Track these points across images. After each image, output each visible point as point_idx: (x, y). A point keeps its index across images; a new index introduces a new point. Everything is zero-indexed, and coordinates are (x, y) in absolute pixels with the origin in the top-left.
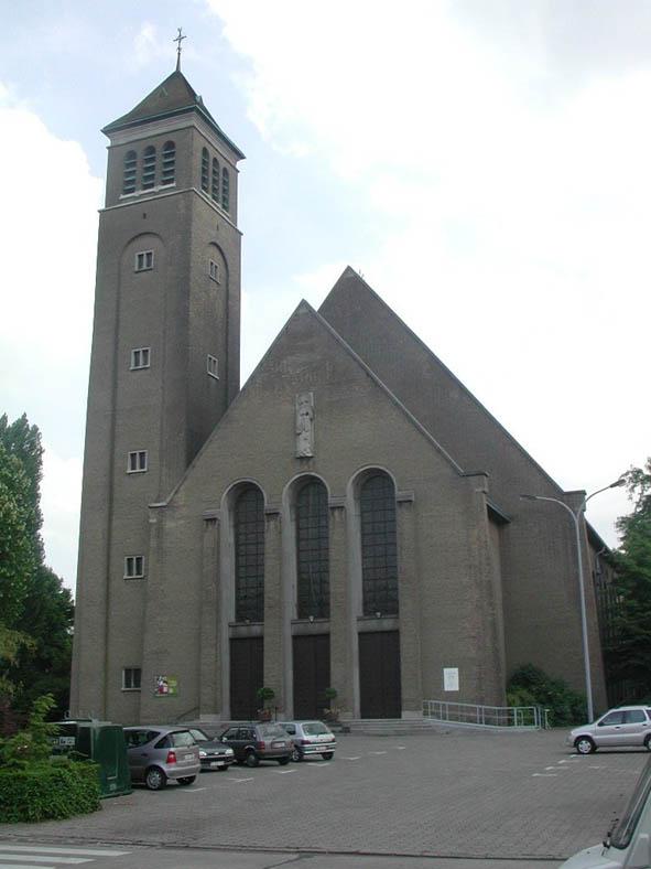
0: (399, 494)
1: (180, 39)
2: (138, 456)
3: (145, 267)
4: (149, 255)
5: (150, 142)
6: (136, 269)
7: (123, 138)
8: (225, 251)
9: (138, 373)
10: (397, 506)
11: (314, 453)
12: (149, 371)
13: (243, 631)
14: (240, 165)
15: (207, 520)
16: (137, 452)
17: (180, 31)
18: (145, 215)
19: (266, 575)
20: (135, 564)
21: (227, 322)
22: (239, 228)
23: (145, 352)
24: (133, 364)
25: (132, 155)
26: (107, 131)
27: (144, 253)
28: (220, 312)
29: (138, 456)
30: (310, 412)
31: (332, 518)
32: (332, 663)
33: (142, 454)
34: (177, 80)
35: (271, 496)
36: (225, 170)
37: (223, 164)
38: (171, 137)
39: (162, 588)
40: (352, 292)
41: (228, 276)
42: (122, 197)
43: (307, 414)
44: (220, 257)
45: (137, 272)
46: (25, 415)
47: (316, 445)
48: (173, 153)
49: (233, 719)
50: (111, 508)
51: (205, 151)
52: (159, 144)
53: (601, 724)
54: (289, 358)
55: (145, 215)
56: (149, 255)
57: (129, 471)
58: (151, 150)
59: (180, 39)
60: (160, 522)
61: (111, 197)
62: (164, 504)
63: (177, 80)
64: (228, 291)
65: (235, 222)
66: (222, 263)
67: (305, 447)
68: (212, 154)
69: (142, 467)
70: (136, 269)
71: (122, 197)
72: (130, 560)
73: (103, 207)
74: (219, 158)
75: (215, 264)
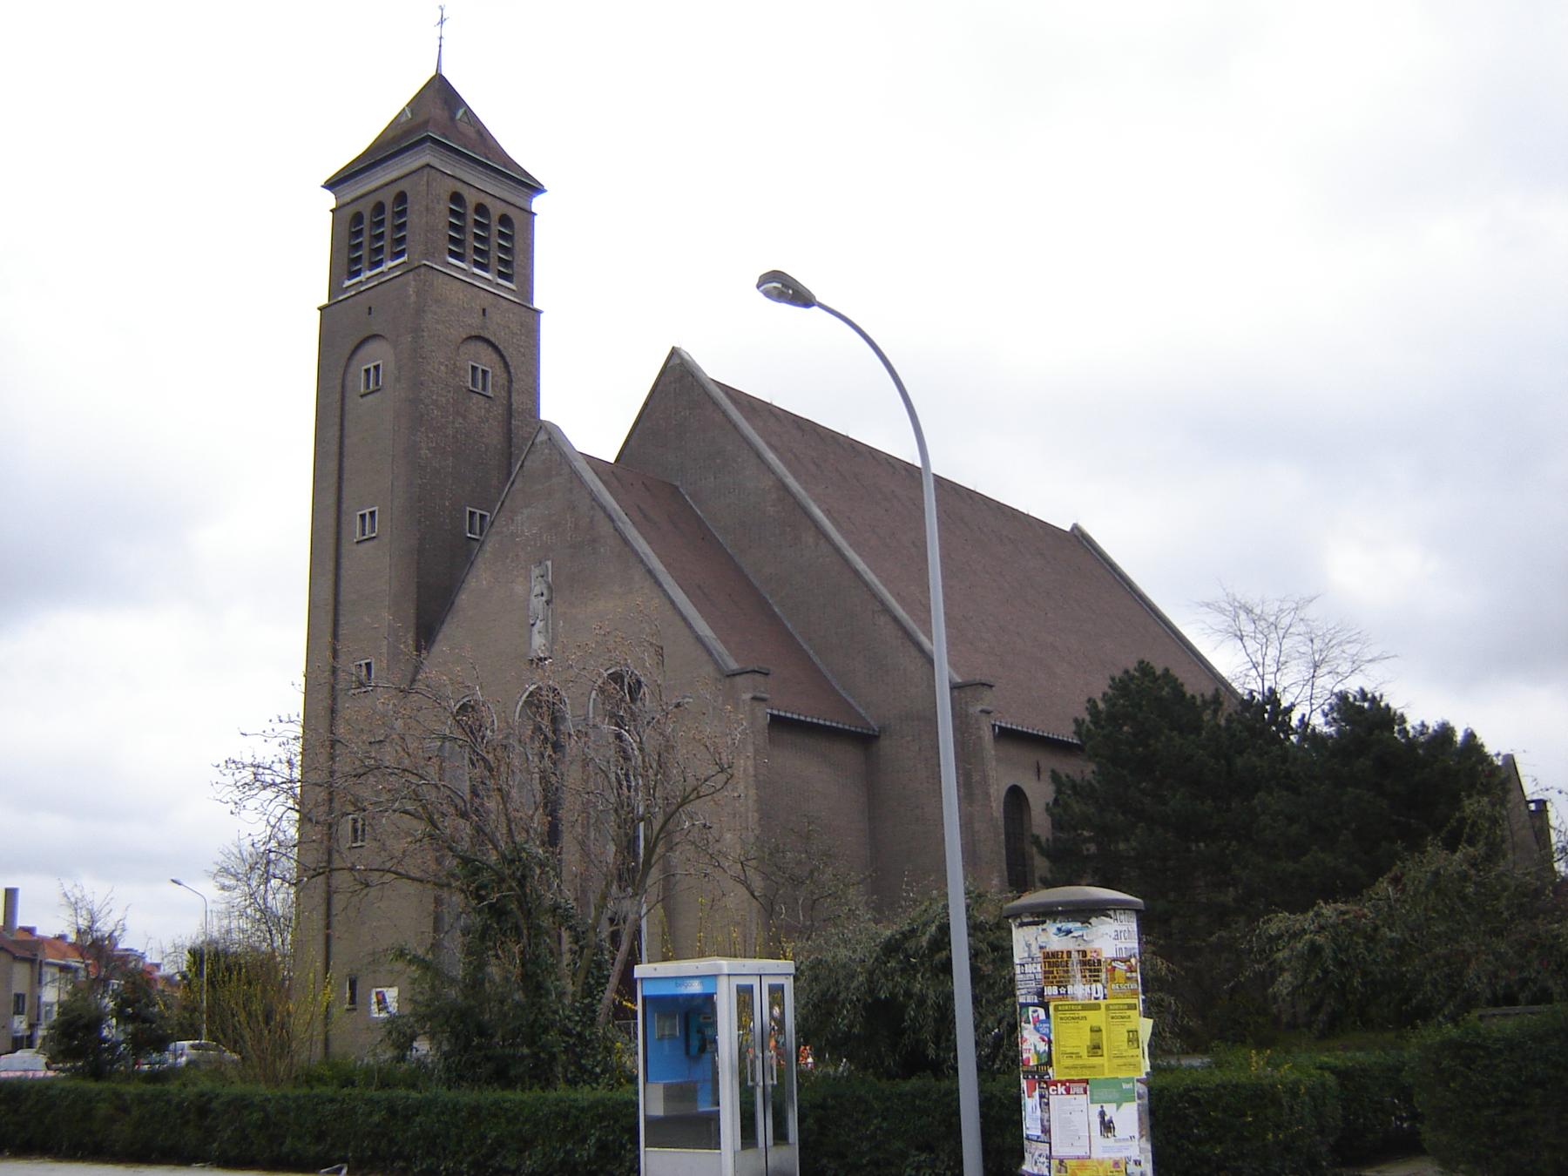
2: (368, 516)
4: (377, 368)
5: (379, 197)
6: (362, 390)
9: (367, 544)
14: (538, 203)
22: (537, 305)
23: (372, 514)
25: (358, 218)
27: (363, 662)
28: (494, 439)
29: (368, 516)
30: (545, 592)
34: (439, 93)
36: (505, 220)
37: (496, 209)
38: (403, 186)
41: (510, 381)
42: (348, 283)
43: (542, 595)
44: (495, 356)
45: (362, 396)
46: (323, 186)
51: (456, 198)
52: (388, 197)
58: (379, 208)
63: (439, 93)
64: (510, 405)
66: (499, 367)
68: (472, 198)
70: (362, 390)
71: (348, 283)
73: (334, 206)
74: (487, 201)
75: (480, 367)
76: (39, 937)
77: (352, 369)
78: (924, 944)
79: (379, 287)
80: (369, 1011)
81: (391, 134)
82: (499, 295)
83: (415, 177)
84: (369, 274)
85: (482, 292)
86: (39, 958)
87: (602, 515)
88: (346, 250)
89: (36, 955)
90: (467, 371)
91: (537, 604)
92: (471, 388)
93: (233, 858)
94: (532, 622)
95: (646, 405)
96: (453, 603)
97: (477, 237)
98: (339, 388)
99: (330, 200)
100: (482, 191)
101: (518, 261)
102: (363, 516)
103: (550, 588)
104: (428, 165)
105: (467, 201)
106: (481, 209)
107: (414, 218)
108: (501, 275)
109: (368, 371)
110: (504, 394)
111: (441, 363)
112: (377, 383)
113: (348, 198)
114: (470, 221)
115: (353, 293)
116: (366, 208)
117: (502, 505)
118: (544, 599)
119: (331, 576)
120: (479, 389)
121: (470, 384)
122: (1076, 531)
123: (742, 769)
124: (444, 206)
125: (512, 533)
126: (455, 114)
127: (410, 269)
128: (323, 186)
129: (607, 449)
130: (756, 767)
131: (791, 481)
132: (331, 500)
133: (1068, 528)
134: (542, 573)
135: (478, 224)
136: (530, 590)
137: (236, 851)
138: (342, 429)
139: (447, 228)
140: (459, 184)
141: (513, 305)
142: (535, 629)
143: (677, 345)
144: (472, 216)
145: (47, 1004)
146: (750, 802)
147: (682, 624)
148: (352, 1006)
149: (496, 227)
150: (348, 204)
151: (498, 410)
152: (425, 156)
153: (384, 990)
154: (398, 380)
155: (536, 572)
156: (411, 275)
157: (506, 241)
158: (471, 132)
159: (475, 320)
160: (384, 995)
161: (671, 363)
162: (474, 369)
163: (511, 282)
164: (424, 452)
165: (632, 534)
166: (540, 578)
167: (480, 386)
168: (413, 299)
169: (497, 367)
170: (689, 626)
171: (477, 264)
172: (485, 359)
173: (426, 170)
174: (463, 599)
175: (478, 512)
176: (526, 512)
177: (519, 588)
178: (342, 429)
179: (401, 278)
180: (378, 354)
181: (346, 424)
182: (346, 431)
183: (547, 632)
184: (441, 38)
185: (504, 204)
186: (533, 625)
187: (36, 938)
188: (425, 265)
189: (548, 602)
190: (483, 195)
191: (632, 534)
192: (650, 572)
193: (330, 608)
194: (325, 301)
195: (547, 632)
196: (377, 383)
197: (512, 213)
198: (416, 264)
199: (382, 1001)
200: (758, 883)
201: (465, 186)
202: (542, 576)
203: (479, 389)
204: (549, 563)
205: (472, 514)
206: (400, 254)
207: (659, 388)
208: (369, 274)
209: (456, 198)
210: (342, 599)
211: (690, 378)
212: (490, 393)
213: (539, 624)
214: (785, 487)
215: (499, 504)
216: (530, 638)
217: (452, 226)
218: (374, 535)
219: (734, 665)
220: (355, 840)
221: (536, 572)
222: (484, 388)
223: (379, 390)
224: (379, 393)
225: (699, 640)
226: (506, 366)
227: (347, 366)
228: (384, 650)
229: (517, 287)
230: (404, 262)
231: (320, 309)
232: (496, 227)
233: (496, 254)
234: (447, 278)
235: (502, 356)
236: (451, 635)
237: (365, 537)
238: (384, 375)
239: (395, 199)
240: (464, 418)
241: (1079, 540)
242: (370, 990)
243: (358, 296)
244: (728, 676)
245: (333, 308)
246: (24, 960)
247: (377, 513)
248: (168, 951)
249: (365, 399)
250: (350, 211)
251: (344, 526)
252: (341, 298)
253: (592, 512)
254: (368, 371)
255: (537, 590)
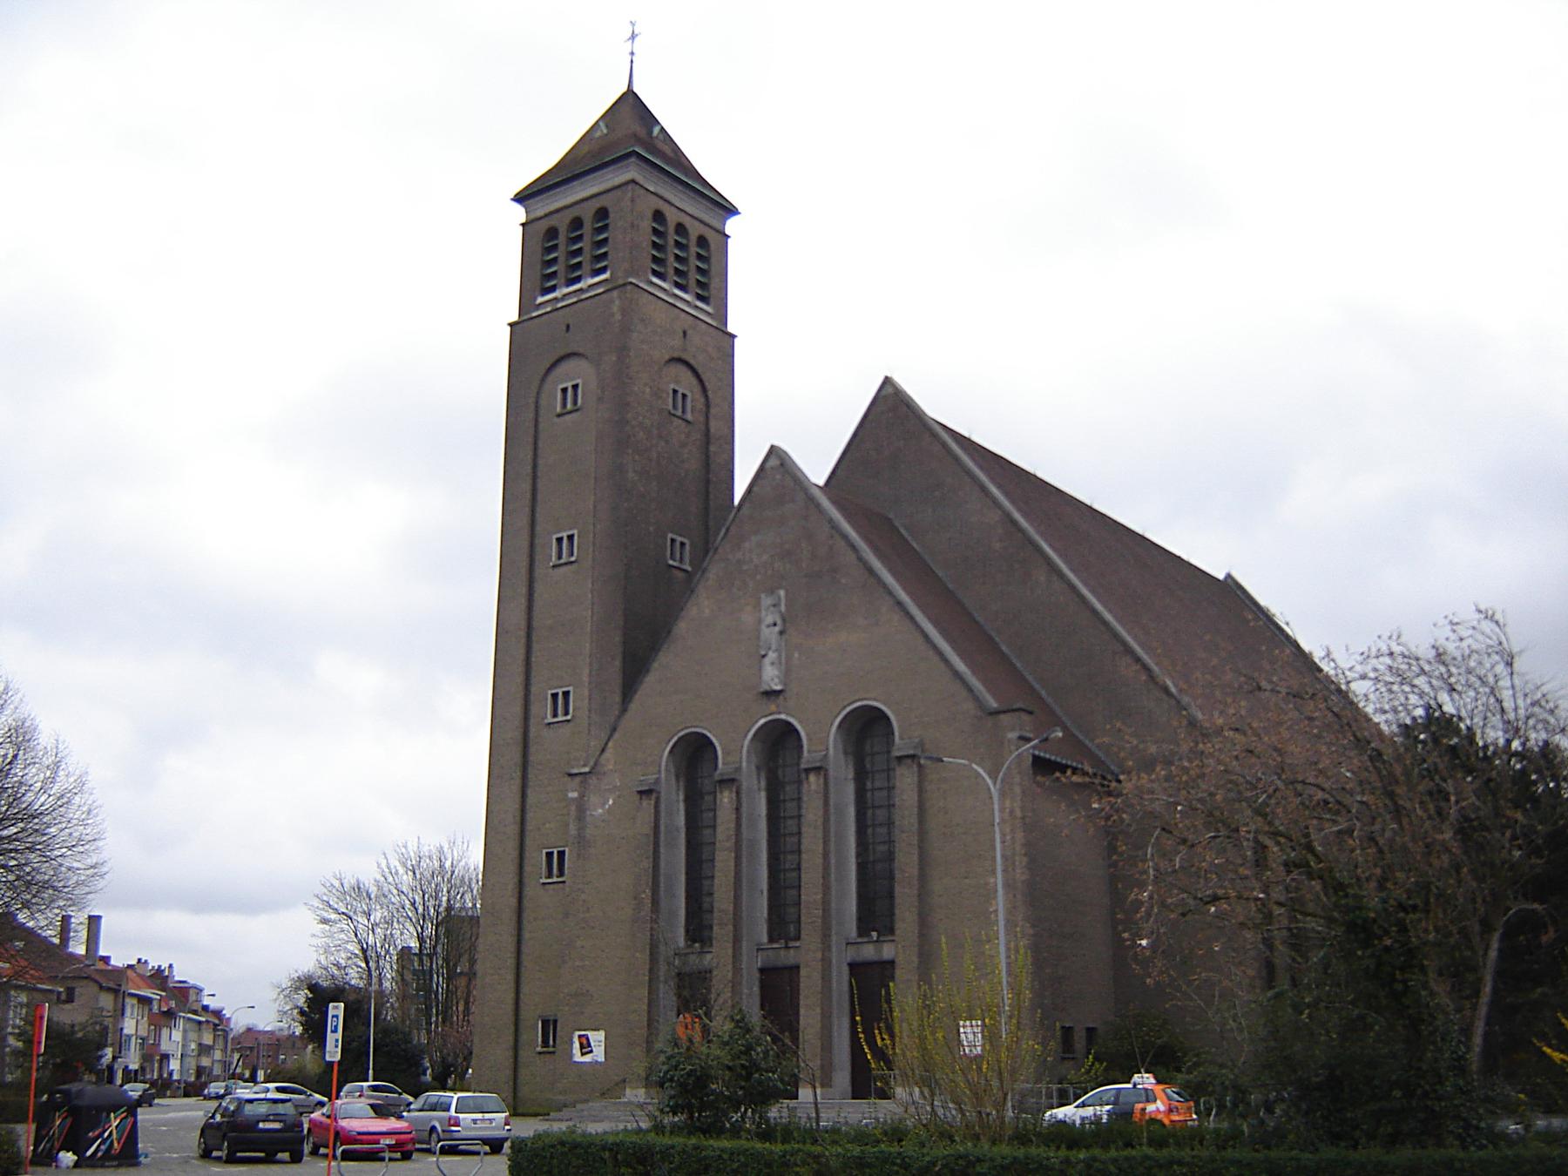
0: (900, 745)
1: (633, 37)
3: (569, 406)
6: (559, 409)
7: (545, 206)
8: (700, 371)
10: (894, 764)
11: (785, 684)
12: (574, 566)
13: (868, 952)
14: (731, 226)
15: (640, 793)
16: (560, 691)
17: (633, 24)
18: (568, 326)
19: (717, 874)
20: (554, 864)
21: (708, 482)
22: (731, 328)
23: (571, 538)
24: (554, 559)
25: (552, 233)
26: (520, 198)
28: (693, 464)
30: (779, 622)
31: (805, 785)
32: (802, 1011)
33: (566, 694)
34: (630, 107)
35: (726, 753)
36: (702, 241)
37: (695, 230)
39: (583, 896)
40: (773, 451)
41: (708, 405)
42: (540, 300)
43: (775, 625)
44: (694, 381)
45: (559, 415)
46: (512, 199)
47: (786, 675)
48: (581, 236)
49: (853, 1098)
50: (524, 777)
51: (658, 216)
52: (587, 212)
53: (1083, 1105)
54: (753, 538)
55: (568, 326)
56: (575, 387)
57: (550, 719)
58: (577, 223)
59: (633, 37)
60: (582, 796)
61: (525, 304)
62: (587, 769)
63: (630, 107)
64: (708, 430)
65: (723, 318)
66: (697, 388)
67: (771, 676)
68: (672, 217)
69: (566, 713)
70: (559, 409)
71: (540, 300)
72: (550, 855)
73: (524, 220)
74: (687, 221)
75: (681, 391)
76: (113, 966)
77: (547, 386)
78: (1508, 1000)
79: (579, 304)
80: (571, 1055)
81: (586, 149)
82: (697, 318)
83: (619, 193)
84: (566, 290)
85: (683, 315)
86: (123, 988)
87: (843, 543)
88: (539, 267)
89: (120, 985)
90: (668, 394)
91: (770, 634)
92: (673, 412)
93: (334, 891)
94: (763, 653)
95: (855, 435)
96: (669, 632)
97: (677, 257)
98: (532, 407)
99: (519, 213)
100: (682, 210)
101: (715, 283)
102: (560, 540)
103: (784, 620)
104: (633, 181)
105: (668, 219)
106: (681, 229)
107: (616, 234)
108: (700, 297)
109: (564, 390)
110: (702, 419)
111: (646, 385)
112: (575, 402)
113: (540, 213)
114: (671, 242)
115: (549, 309)
116: (562, 223)
117: (726, 534)
118: (777, 629)
119: (523, 601)
120: (679, 413)
121: (670, 407)
122: (1229, 580)
123: (1007, 810)
124: (647, 224)
125: (739, 561)
126: (652, 132)
127: (612, 287)
128: (512, 199)
129: (821, 482)
130: (1023, 808)
131: (1017, 516)
132: (523, 521)
133: (1221, 576)
134: (774, 602)
135: (678, 244)
136: (760, 621)
137: (337, 884)
138: (535, 449)
139: (650, 247)
140: (661, 202)
141: (711, 330)
142: (767, 661)
143: (889, 375)
144: (672, 236)
145: (127, 1036)
146: (1018, 848)
147: (936, 659)
148: (545, 1049)
149: (694, 249)
150: (541, 218)
151: (697, 436)
152: (631, 172)
153: (589, 1033)
154: (600, 399)
155: (767, 601)
156: (615, 293)
157: (703, 262)
158: (667, 150)
159: (677, 342)
160: (588, 1039)
161: (884, 392)
162: (675, 392)
163: (708, 303)
164: (631, 475)
165: (877, 564)
166: (772, 609)
167: (680, 410)
168: (618, 317)
169: (695, 390)
170: (946, 661)
171: (678, 285)
172: (687, 383)
173: (630, 187)
174: (682, 627)
175: (679, 539)
176: (754, 539)
177: (747, 618)
178: (535, 449)
179: (604, 296)
180: (577, 373)
181: (540, 444)
182: (540, 451)
183: (780, 663)
184: (632, 53)
185: (702, 226)
186: (764, 656)
187: (110, 968)
188: (631, 283)
189: (781, 633)
190: (683, 214)
191: (877, 564)
192: (900, 604)
193: (523, 633)
194: (515, 317)
195: (780, 663)
196: (575, 402)
197: (710, 235)
198: (621, 282)
199: (586, 1047)
200: (429, 930)
201: (667, 205)
202: (774, 606)
203: (679, 413)
204: (782, 593)
205: (673, 541)
206: (603, 270)
207: (870, 417)
208: (566, 290)
209: (658, 216)
210: (535, 624)
211: (905, 408)
212: (689, 417)
213: (772, 655)
214: (1014, 522)
215: (723, 531)
216: (760, 669)
217: (655, 245)
218: (573, 559)
219: (994, 704)
220: (550, 875)
221: (767, 601)
222: (683, 412)
223: (577, 410)
224: (578, 413)
225: (957, 675)
226: (704, 390)
227: (543, 380)
228: (586, 679)
229: (714, 308)
230: (606, 280)
231: (511, 325)
232: (694, 249)
233: (694, 276)
234: (651, 297)
235: (701, 381)
236: (667, 665)
237: (562, 561)
238: (584, 394)
239: (597, 212)
240: (667, 442)
241: (1230, 593)
242: (573, 1033)
243: (556, 313)
244: (991, 714)
245: (525, 324)
246: (109, 989)
247: (576, 537)
248: (284, 986)
249: (562, 418)
250: (543, 226)
251: (538, 549)
252: (534, 314)
253: (830, 542)
254: (564, 390)
255: (769, 619)
